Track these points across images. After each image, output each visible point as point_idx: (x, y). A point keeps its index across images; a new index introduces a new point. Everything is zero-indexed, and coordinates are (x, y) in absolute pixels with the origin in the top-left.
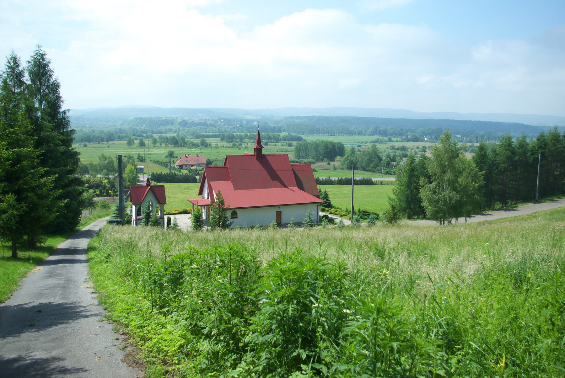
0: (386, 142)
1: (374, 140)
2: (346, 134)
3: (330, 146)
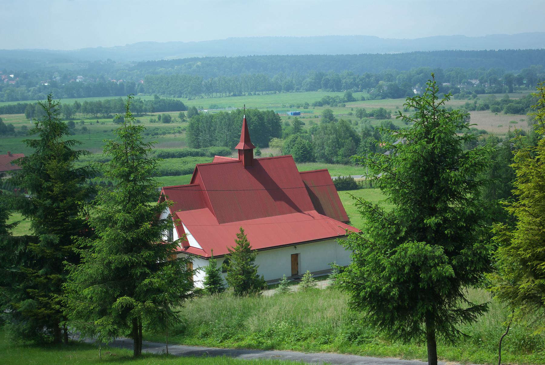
0: (343, 102)
1: (320, 100)
2: (262, 91)
3: (254, 119)
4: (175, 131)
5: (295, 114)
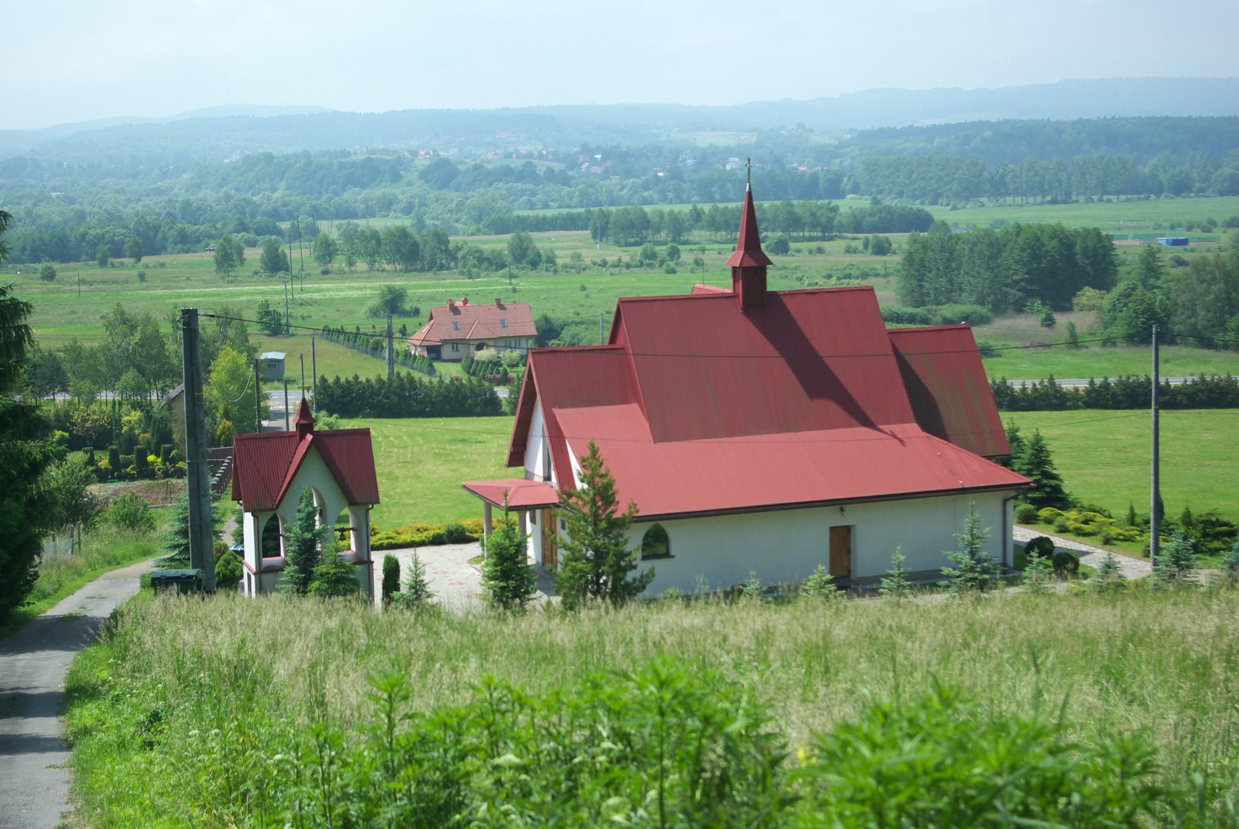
2: (1118, 193)
3: (1051, 245)
4: (890, 271)
5: (1176, 243)
